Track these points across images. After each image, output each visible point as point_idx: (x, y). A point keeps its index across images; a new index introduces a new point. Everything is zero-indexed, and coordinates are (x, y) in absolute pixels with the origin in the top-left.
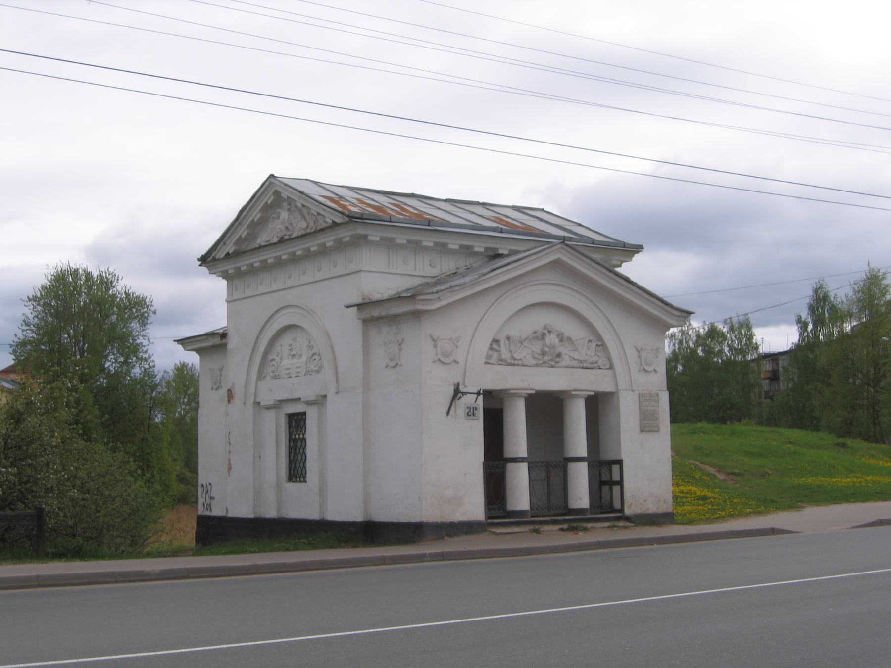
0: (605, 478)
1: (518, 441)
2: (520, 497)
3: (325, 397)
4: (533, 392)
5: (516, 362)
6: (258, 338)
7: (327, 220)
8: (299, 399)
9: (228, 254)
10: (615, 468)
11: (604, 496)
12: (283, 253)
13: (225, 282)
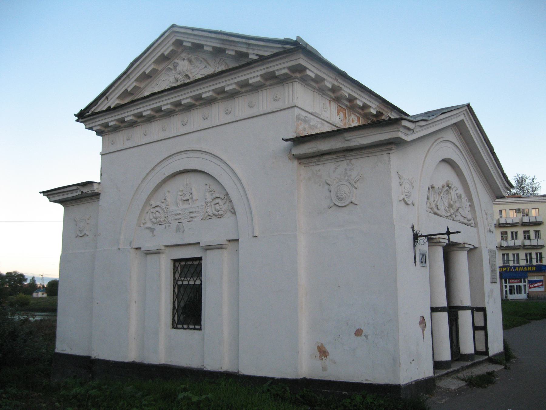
6: (208, 152)
9: (109, 107)
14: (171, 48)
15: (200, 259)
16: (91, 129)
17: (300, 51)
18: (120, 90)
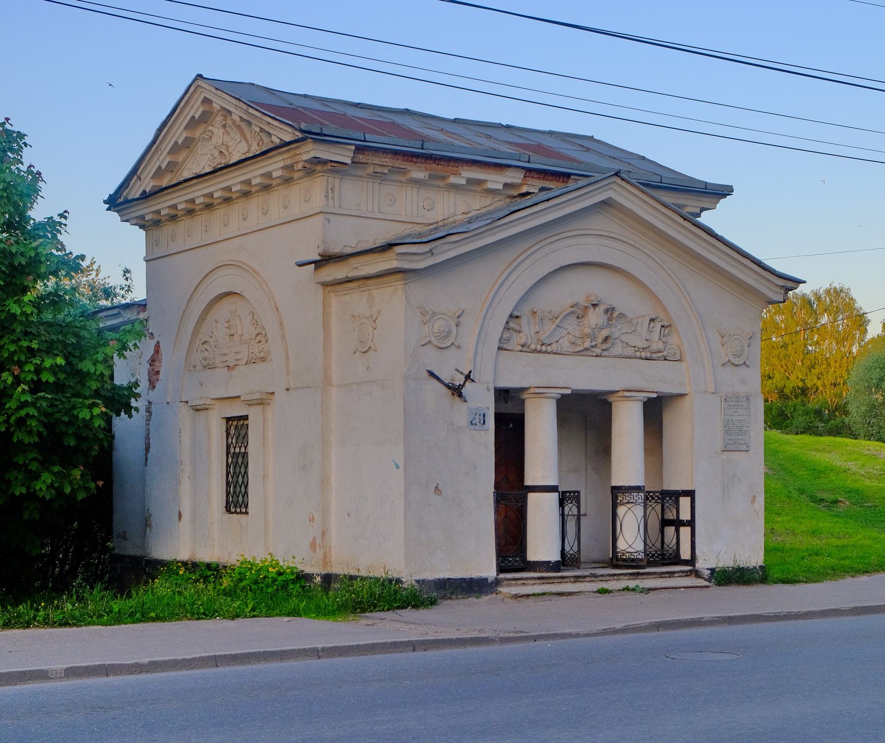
0: (670, 515)
1: (543, 458)
3: (466, 401)
4: (569, 392)
5: (544, 348)
7: (274, 139)
8: (239, 397)
9: (144, 192)
10: (685, 502)
11: (667, 540)
12: (215, 187)
13: (142, 233)
14: (201, 109)
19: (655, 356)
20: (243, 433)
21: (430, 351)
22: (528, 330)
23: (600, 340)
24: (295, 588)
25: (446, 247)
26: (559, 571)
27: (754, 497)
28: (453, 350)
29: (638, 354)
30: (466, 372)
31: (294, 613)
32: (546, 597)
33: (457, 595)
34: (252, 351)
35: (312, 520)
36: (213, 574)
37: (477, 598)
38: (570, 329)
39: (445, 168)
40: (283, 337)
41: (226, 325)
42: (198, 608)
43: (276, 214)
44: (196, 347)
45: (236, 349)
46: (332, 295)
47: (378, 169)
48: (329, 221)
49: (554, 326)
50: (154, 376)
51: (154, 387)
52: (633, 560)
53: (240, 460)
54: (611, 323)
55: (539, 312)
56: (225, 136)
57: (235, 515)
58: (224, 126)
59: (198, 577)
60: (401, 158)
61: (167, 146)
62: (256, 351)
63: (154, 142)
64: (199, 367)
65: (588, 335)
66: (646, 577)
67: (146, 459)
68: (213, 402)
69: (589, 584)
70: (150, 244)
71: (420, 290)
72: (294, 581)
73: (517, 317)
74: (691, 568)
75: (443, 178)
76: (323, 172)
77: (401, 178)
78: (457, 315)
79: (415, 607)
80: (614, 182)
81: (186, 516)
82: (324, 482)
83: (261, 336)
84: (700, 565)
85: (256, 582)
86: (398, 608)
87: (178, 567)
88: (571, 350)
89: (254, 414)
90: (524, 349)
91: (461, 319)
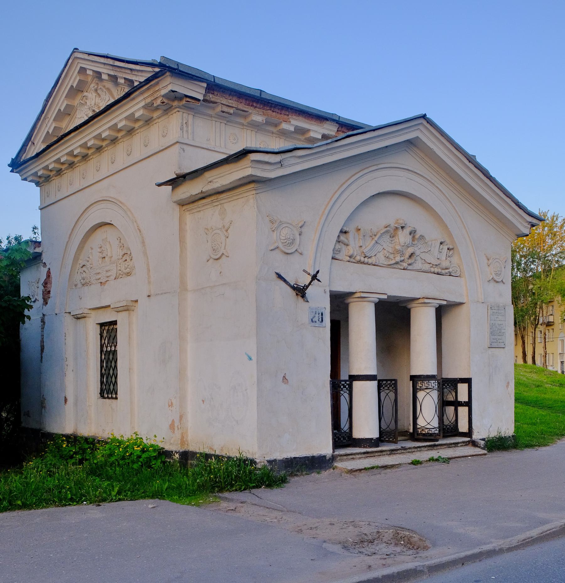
0: (451, 398)
1: (363, 354)
2: (366, 426)
3: (307, 301)
8: (109, 306)
10: (463, 388)
14: (78, 79)
15: (115, 323)
16: (25, 179)
17: (168, 74)
18: (43, 134)
19: (443, 271)
20: (113, 335)
21: (278, 255)
22: (354, 245)
23: (407, 256)
24: (157, 464)
25: (293, 161)
26: (377, 446)
27: (508, 383)
28: (297, 255)
29: (432, 270)
30: (312, 273)
31: (157, 495)
32: (374, 470)
33: (302, 471)
34: (119, 268)
35: (171, 405)
36: (89, 448)
37: (318, 473)
38: (385, 246)
39: (279, 116)
40: (145, 254)
41: (99, 250)
42: (66, 492)
43: (138, 152)
44: (77, 271)
45: (107, 268)
46: (187, 213)
47: (226, 109)
48: (184, 150)
49: (374, 242)
50: (46, 294)
51: (47, 303)
52: (431, 435)
53: (111, 357)
54: (414, 243)
55: (362, 229)
56: (97, 98)
57: (107, 400)
58: (96, 90)
59: (77, 449)
60: (244, 101)
61: (52, 114)
62: (123, 269)
63: (42, 112)
64: (80, 285)
65: (398, 252)
66: (439, 447)
67: (42, 357)
68: (89, 312)
69: (401, 456)
70: (43, 197)
71: (269, 199)
72: (156, 458)
73: (346, 232)
74: (469, 439)
75: (276, 125)
76: (179, 107)
77: (242, 120)
78: (300, 225)
79: (269, 486)
80: (421, 123)
81: (71, 400)
82: (181, 374)
83: (127, 255)
84: (476, 436)
85: (123, 458)
86: (254, 487)
87: (63, 441)
88: (386, 263)
89: (121, 318)
90: (352, 260)
91: (303, 230)
